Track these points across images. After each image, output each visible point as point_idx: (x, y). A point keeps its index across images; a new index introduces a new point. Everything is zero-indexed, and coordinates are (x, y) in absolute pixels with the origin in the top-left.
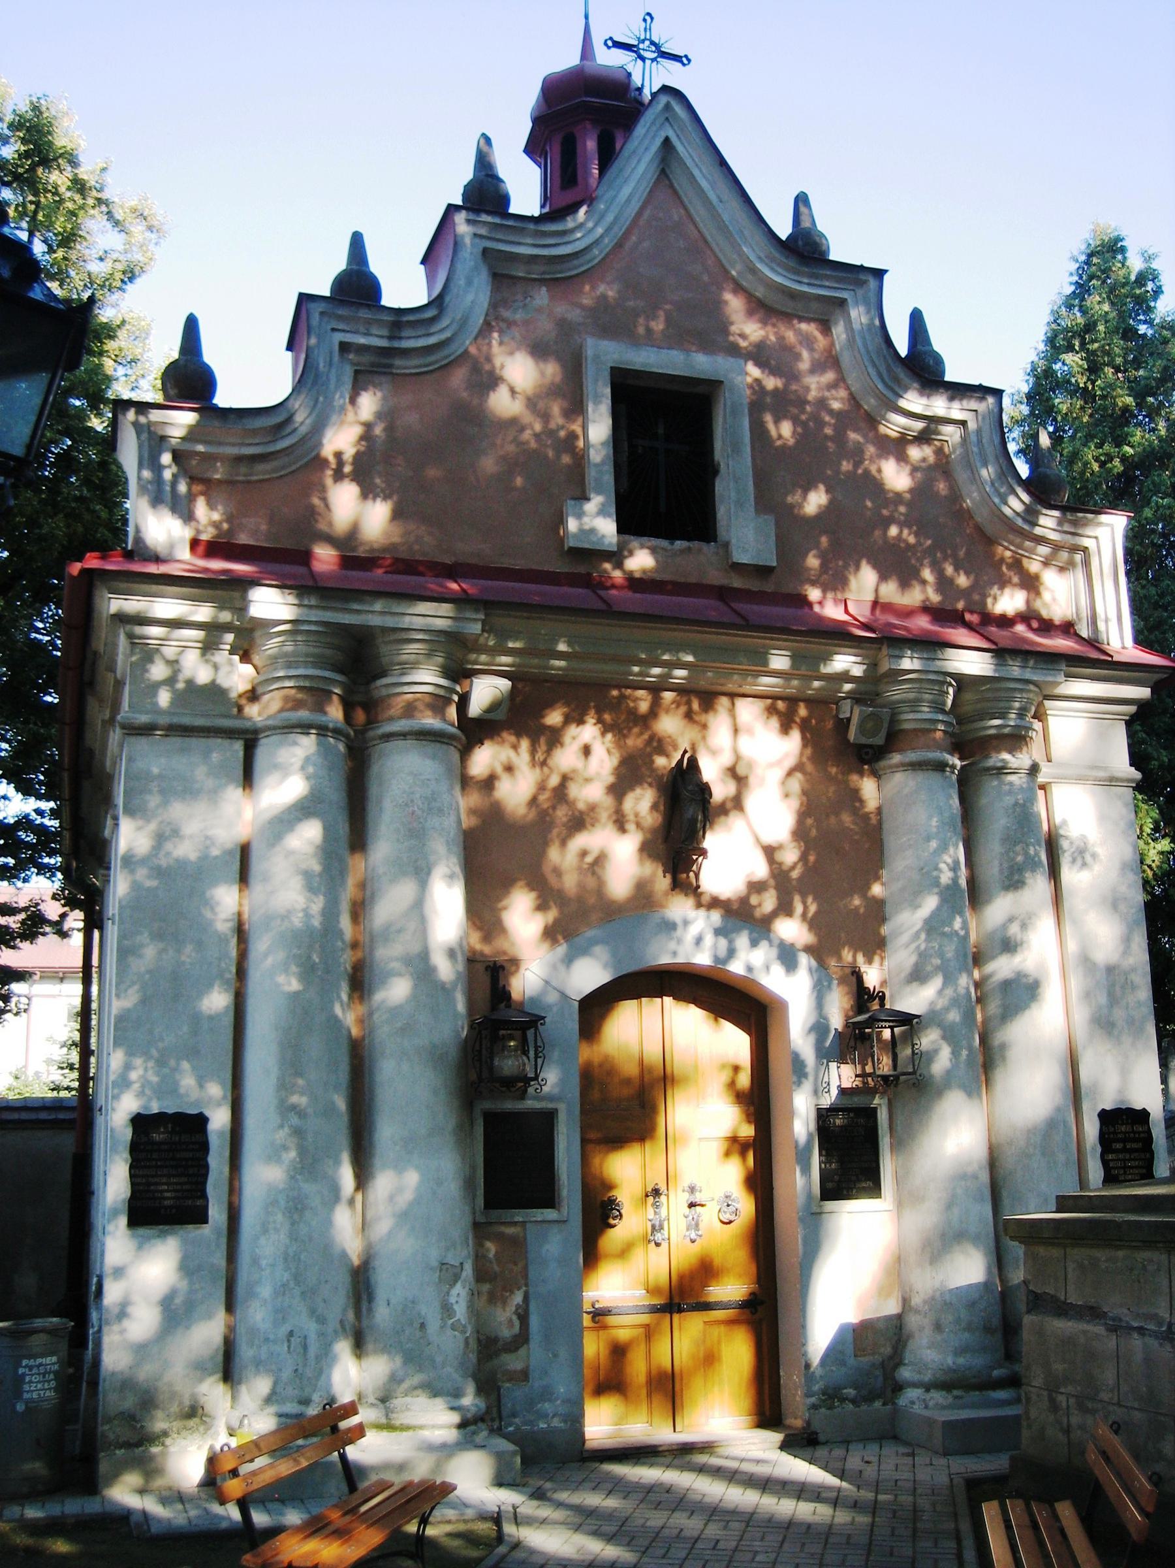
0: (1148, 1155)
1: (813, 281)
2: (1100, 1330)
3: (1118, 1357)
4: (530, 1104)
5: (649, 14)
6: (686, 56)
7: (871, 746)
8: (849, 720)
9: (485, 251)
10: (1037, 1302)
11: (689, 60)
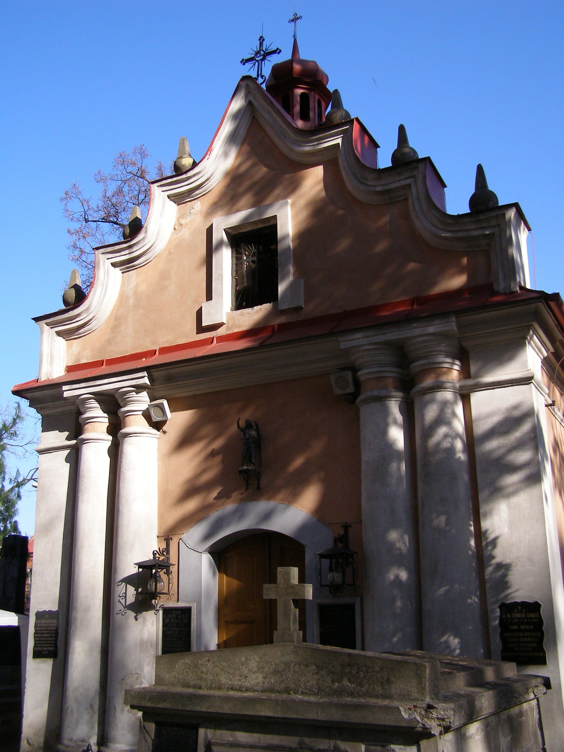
0: (539, 634)
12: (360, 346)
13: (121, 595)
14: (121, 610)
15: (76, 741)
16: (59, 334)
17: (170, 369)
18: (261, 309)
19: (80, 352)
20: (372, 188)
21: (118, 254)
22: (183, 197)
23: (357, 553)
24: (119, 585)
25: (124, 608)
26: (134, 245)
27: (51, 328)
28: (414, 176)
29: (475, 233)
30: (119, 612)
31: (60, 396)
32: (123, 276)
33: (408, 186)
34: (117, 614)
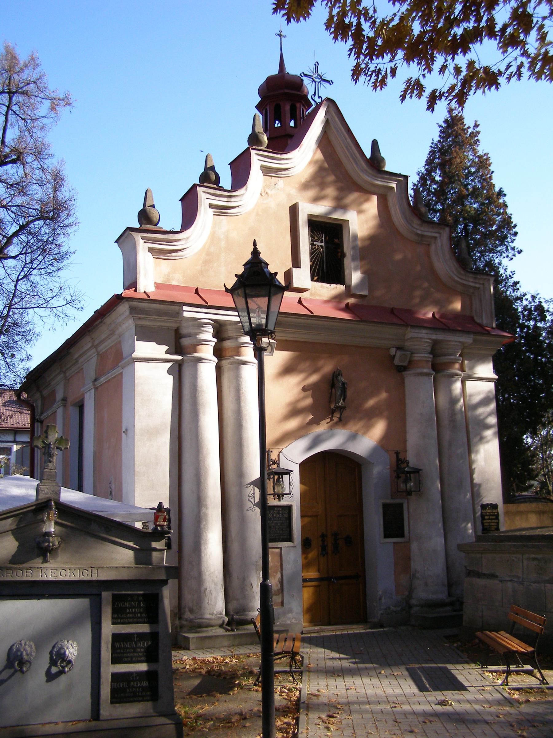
0: (497, 521)
1: (383, 180)
2: (497, 582)
3: (502, 591)
4: (283, 502)
5: (317, 62)
6: (331, 81)
7: (402, 366)
8: (394, 356)
9: (262, 166)
10: (470, 573)
11: (333, 83)
12: (421, 338)
13: (250, 495)
14: (251, 507)
15: (216, 615)
16: (151, 250)
17: (284, 317)
18: (336, 287)
19: (169, 273)
20: (415, 230)
21: (217, 198)
22: (270, 171)
23: (292, 471)
24: (247, 487)
25: (254, 505)
26: (234, 196)
27: (144, 242)
28: (440, 233)
29: (472, 284)
30: (249, 509)
31: (179, 313)
32: (153, 202)
33: (435, 238)
34: (248, 510)
